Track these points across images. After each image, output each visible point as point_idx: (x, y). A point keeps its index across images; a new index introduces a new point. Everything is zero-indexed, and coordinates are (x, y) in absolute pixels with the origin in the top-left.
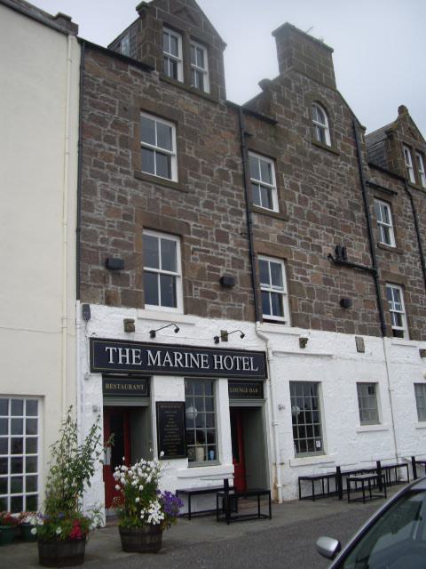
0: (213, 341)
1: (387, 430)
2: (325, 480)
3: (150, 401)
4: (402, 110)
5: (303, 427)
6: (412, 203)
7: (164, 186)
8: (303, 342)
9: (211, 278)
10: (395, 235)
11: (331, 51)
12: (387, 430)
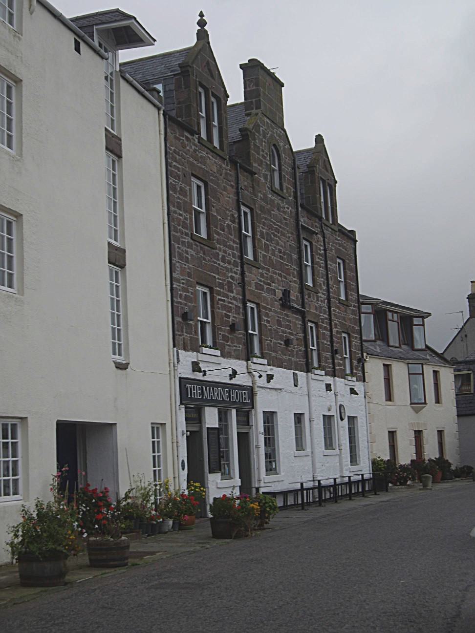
0: (229, 378)
1: (308, 456)
2: (311, 491)
3: (201, 427)
4: (319, 139)
5: (159, 467)
6: (324, 240)
7: (204, 245)
8: (270, 378)
9: (281, 338)
10: (254, 246)
11: (282, 85)
12: (308, 456)
